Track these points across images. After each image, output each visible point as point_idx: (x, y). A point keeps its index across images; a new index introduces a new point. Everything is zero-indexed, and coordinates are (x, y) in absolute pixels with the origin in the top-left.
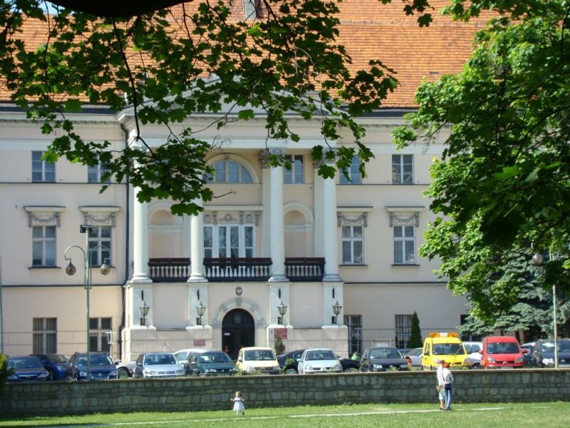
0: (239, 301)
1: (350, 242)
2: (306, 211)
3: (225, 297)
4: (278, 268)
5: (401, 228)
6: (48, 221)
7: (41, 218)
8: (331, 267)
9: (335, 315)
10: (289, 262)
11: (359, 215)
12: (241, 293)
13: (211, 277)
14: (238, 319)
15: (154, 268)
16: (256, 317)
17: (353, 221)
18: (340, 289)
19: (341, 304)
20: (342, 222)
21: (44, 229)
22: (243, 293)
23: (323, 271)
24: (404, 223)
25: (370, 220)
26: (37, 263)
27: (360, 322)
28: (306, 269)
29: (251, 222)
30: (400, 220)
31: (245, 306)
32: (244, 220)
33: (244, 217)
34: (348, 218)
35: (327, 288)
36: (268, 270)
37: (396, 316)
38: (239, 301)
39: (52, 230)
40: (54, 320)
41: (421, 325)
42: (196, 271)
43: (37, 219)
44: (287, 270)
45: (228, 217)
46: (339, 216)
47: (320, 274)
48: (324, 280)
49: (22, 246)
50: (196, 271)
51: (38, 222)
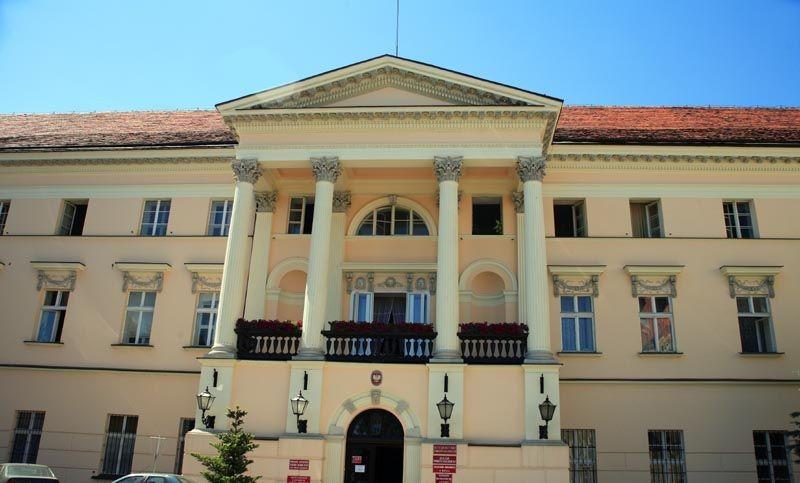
0: (375, 395)
1: (580, 311)
2: (506, 275)
4: (447, 339)
5: (747, 300)
6: (146, 284)
7: (53, 279)
9: (543, 423)
10: (467, 332)
11: (661, 279)
12: (380, 381)
13: (471, 356)
14: (377, 426)
15: (467, 341)
17: (577, 288)
19: (555, 401)
20: (561, 290)
21: (144, 294)
22: (383, 381)
23: (524, 345)
24: (654, 292)
25: (602, 285)
27: (679, 442)
28: (495, 341)
29: (363, 288)
30: (647, 288)
32: (414, 285)
33: (414, 282)
34: (568, 284)
35: (530, 373)
36: (431, 346)
37: (593, 431)
38: (375, 395)
39: (151, 297)
40: (41, 416)
41: (42, 444)
43: (135, 282)
44: (463, 346)
45: (391, 281)
46: (554, 279)
47: (519, 355)
48: (525, 361)
49: (31, 309)
51: (204, 286)
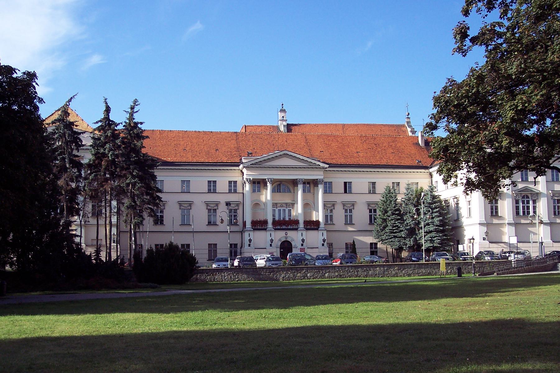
3: (279, 236)
8: (322, 226)
10: (275, 223)
16: (293, 244)
18: (325, 233)
26: (209, 223)
31: (289, 240)
35: (320, 233)
42: (270, 225)
50: (270, 225)
